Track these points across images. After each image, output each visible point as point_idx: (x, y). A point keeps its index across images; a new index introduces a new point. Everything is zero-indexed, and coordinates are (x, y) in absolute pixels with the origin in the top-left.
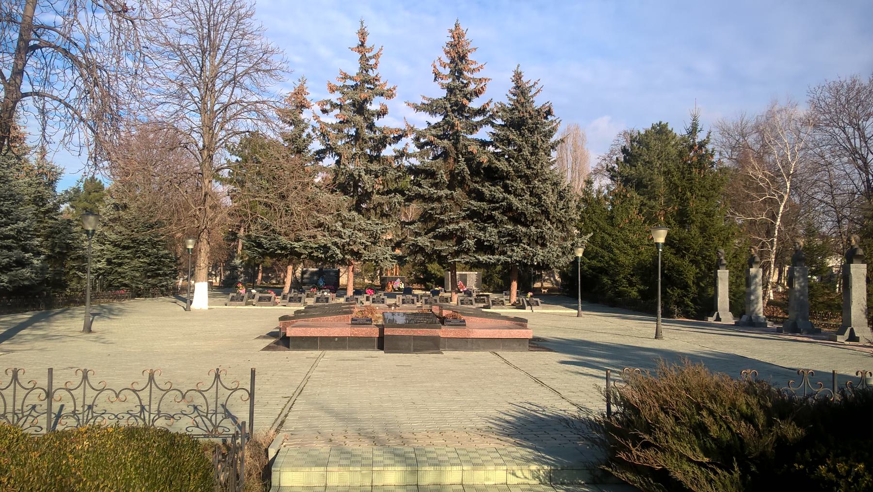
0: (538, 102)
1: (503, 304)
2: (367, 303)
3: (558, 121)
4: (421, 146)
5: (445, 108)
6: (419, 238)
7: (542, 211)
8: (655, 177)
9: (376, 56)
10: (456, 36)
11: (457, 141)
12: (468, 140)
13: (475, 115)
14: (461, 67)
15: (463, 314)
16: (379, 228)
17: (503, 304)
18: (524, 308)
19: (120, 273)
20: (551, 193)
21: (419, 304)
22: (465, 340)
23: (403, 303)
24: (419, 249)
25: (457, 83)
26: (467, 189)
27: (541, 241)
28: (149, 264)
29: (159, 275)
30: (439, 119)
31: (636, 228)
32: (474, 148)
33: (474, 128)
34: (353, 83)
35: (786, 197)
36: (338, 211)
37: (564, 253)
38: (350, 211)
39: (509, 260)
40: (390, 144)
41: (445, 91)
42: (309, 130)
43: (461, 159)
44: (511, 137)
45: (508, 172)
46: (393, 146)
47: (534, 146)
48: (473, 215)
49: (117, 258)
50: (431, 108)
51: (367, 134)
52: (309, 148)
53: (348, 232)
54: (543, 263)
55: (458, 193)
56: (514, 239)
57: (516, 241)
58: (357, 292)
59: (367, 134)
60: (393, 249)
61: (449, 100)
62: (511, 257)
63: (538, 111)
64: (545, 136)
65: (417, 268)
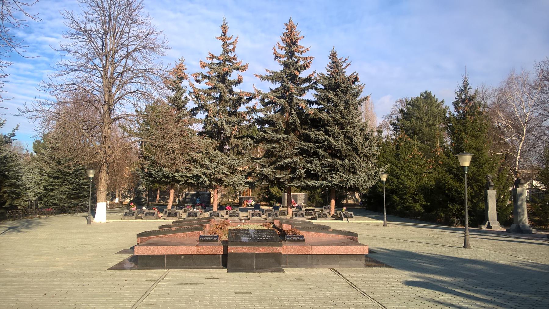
0: (348, 73)
1: (326, 217)
2: (226, 216)
3: (362, 85)
4: (265, 105)
5: (283, 78)
6: (265, 169)
7: (353, 148)
8: (424, 128)
9: (234, 43)
10: (290, 28)
11: (291, 100)
12: (299, 100)
13: (304, 83)
14: (293, 49)
15: (302, 229)
16: (236, 162)
17: (326, 217)
18: (342, 220)
19: (51, 196)
20: (359, 136)
21: (264, 217)
22: (305, 256)
23: (253, 216)
24: (265, 177)
25: (290, 60)
26: (298, 134)
27: (353, 170)
28: (73, 190)
29: (79, 197)
30: (278, 85)
31: (417, 161)
32: (303, 105)
33: (302, 92)
34: (218, 62)
35: (523, 138)
36: (206, 150)
37: (369, 179)
38: (215, 150)
39: (330, 184)
40: (244, 104)
41: (283, 66)
42: (186, 94)
43: (293, 112)
44: (330, 96)
45: (328, 121)
46: (246, 105)
47: (347, 103)
48: (302, 152)
49: (50, 185)
50: (273, 78)
51: (228, 96)
52: (186, 106)
53: (213, 165)
54: (354, 186)
55: (292, 136)
56: (333, 169)
57: (334, 170)
58: (221, 207)
59: (228, 96)
60: (246, 177)
61: (285, 72)
62: (331, 182)
63: (349, 79)
64: (354, 96)
65: (263, 191)
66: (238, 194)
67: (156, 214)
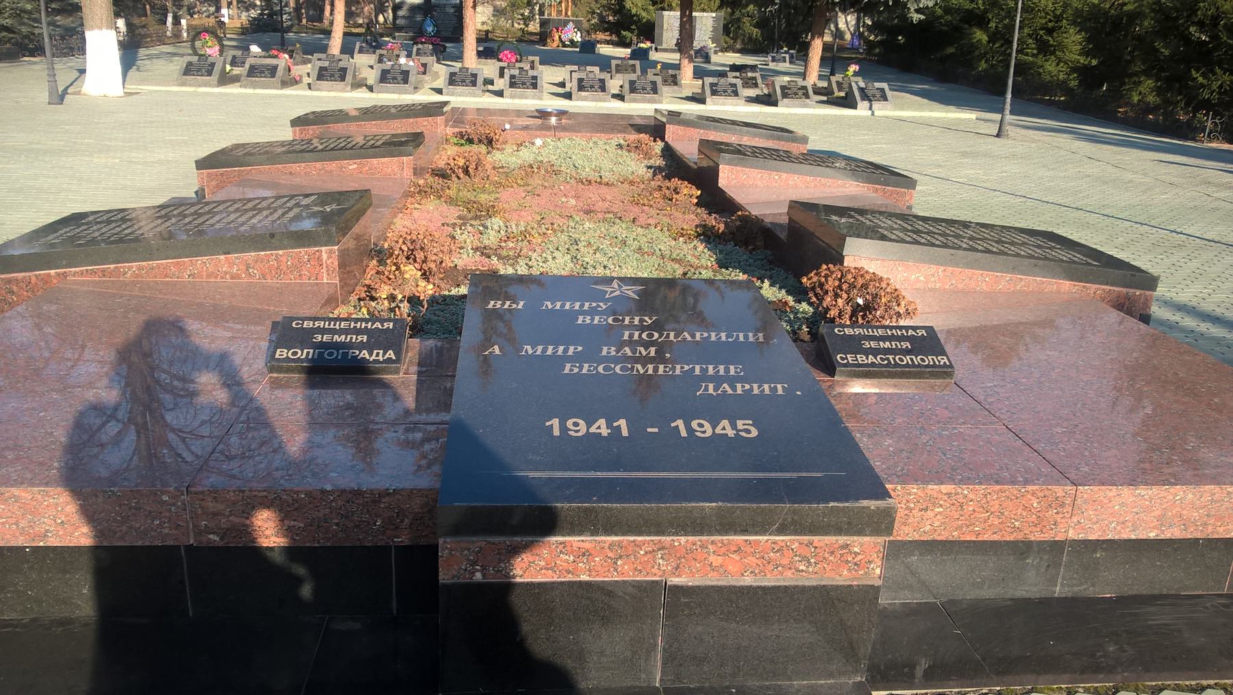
18: (853, 106)
66: (537, 8)
67: (280, 72)
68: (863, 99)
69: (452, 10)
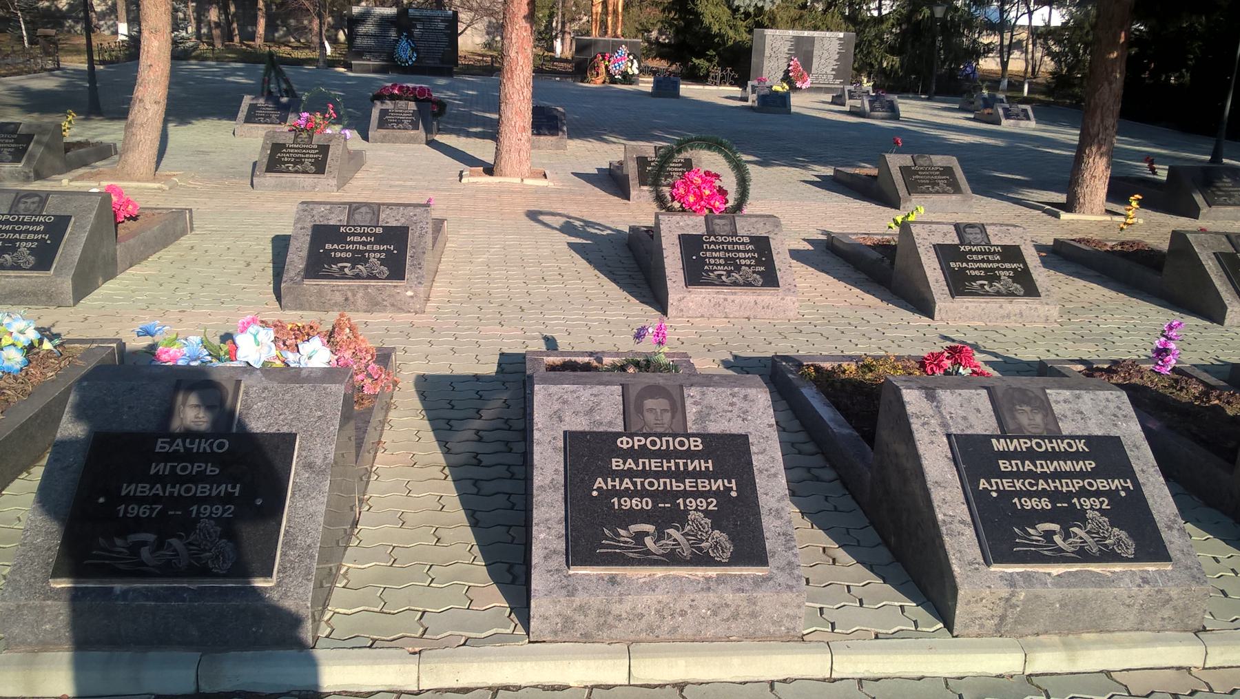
68: (643, 182)
69: (442, 25)
